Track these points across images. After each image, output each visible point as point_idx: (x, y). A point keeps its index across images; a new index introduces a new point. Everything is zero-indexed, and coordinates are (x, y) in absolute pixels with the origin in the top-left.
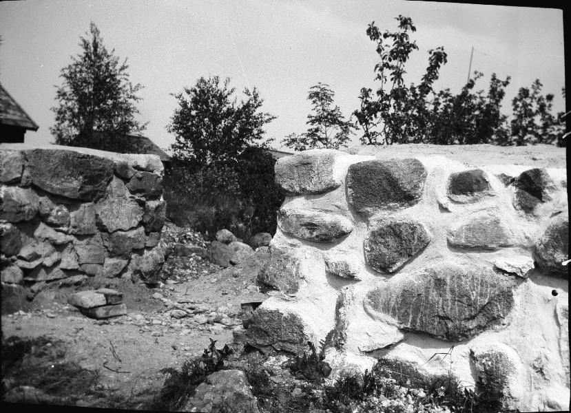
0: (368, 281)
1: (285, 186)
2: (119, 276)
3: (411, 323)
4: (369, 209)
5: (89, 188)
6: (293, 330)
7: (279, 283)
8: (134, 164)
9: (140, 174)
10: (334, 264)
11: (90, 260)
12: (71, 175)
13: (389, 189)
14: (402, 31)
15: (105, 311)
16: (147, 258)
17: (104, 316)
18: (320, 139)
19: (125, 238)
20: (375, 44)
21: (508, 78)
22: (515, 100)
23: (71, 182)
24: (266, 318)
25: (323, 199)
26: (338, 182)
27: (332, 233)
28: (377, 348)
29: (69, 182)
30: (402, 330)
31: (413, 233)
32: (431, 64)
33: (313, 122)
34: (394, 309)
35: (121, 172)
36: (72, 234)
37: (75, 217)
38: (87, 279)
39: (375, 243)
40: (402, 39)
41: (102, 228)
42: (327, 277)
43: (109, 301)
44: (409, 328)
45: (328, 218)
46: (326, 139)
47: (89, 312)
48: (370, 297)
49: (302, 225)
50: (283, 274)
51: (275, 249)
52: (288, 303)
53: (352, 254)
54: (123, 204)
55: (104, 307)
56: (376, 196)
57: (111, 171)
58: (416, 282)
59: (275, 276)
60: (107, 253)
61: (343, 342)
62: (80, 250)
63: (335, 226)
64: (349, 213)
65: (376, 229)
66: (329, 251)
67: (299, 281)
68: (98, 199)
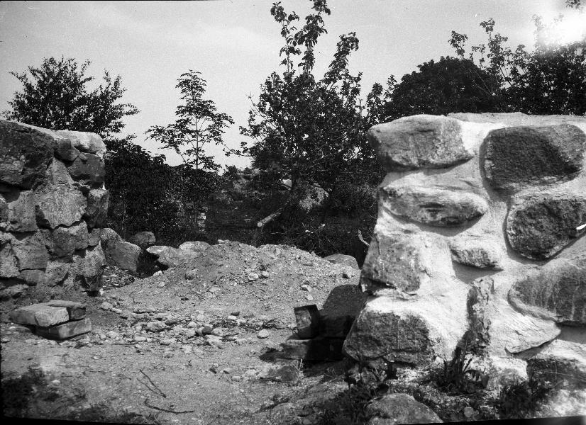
0: (511, 272)
1: (396, 159)
2: (60, 283)
3: (574, 316)
4: (514, 185)
5: (30, 172)
6: (414, 335)
7: (393, 278)
8: (78, 145)
9: (83, 156)
10: (466, 253)
11: (30, 265)
12: (11, 154)
13: (544, 159)
14: (316, 13)
15: (69, 330)
16: (89, 260)
17: (69, 336)
18: (190, 132)
19: (67, 236)
20: (280, 26)
21: (360, 74)
22: (370, 96)
23: (11, 163)
24: (378, 323)
25: (451, 174)
26: (471, 152)
27: (465, 214)
28: (530, 347)
29: (9, 163)
30: (558, 325)
31: (575, 212)
32: (339, 50)
33: (183, 112)
34: (550, 301)
35: (63, 153)
36: (10, 231)
37: (14, 210)
38: (27, 289)
39: (524, 225)
40: (315, 22)
41: (43, 223)
42: (454, 268)
43: (73, 316)
44: (570, 322)
45: (456, 197)
46: (197, 131)
47: (50, 333)
48: (518, 289)
49: (421, 206)
50: (397, 267)
51: (383, 236)
52: (405, 302)
53: (487, 238)
54: (66, 193)
55: (68, 324)
56: (525, 169)
57: (52, 151)
58: (578, 268)
59: (387, 271)
60: (48, 255)
61: (483, 345)
62: (19, 253)
63: (466, 207)
64: (484, 191)
65: (523, 208)
66: (455, 237)
67: (420, 275)
68: (36, 186)
